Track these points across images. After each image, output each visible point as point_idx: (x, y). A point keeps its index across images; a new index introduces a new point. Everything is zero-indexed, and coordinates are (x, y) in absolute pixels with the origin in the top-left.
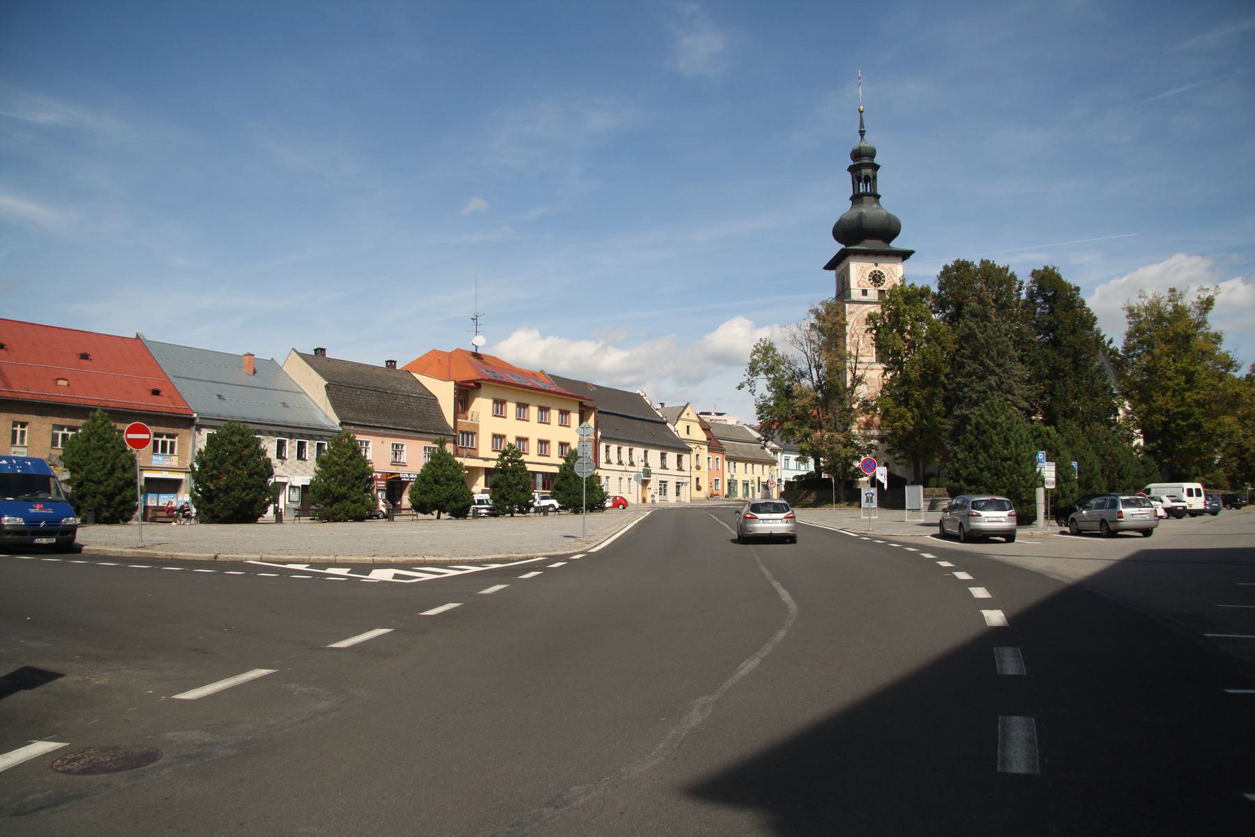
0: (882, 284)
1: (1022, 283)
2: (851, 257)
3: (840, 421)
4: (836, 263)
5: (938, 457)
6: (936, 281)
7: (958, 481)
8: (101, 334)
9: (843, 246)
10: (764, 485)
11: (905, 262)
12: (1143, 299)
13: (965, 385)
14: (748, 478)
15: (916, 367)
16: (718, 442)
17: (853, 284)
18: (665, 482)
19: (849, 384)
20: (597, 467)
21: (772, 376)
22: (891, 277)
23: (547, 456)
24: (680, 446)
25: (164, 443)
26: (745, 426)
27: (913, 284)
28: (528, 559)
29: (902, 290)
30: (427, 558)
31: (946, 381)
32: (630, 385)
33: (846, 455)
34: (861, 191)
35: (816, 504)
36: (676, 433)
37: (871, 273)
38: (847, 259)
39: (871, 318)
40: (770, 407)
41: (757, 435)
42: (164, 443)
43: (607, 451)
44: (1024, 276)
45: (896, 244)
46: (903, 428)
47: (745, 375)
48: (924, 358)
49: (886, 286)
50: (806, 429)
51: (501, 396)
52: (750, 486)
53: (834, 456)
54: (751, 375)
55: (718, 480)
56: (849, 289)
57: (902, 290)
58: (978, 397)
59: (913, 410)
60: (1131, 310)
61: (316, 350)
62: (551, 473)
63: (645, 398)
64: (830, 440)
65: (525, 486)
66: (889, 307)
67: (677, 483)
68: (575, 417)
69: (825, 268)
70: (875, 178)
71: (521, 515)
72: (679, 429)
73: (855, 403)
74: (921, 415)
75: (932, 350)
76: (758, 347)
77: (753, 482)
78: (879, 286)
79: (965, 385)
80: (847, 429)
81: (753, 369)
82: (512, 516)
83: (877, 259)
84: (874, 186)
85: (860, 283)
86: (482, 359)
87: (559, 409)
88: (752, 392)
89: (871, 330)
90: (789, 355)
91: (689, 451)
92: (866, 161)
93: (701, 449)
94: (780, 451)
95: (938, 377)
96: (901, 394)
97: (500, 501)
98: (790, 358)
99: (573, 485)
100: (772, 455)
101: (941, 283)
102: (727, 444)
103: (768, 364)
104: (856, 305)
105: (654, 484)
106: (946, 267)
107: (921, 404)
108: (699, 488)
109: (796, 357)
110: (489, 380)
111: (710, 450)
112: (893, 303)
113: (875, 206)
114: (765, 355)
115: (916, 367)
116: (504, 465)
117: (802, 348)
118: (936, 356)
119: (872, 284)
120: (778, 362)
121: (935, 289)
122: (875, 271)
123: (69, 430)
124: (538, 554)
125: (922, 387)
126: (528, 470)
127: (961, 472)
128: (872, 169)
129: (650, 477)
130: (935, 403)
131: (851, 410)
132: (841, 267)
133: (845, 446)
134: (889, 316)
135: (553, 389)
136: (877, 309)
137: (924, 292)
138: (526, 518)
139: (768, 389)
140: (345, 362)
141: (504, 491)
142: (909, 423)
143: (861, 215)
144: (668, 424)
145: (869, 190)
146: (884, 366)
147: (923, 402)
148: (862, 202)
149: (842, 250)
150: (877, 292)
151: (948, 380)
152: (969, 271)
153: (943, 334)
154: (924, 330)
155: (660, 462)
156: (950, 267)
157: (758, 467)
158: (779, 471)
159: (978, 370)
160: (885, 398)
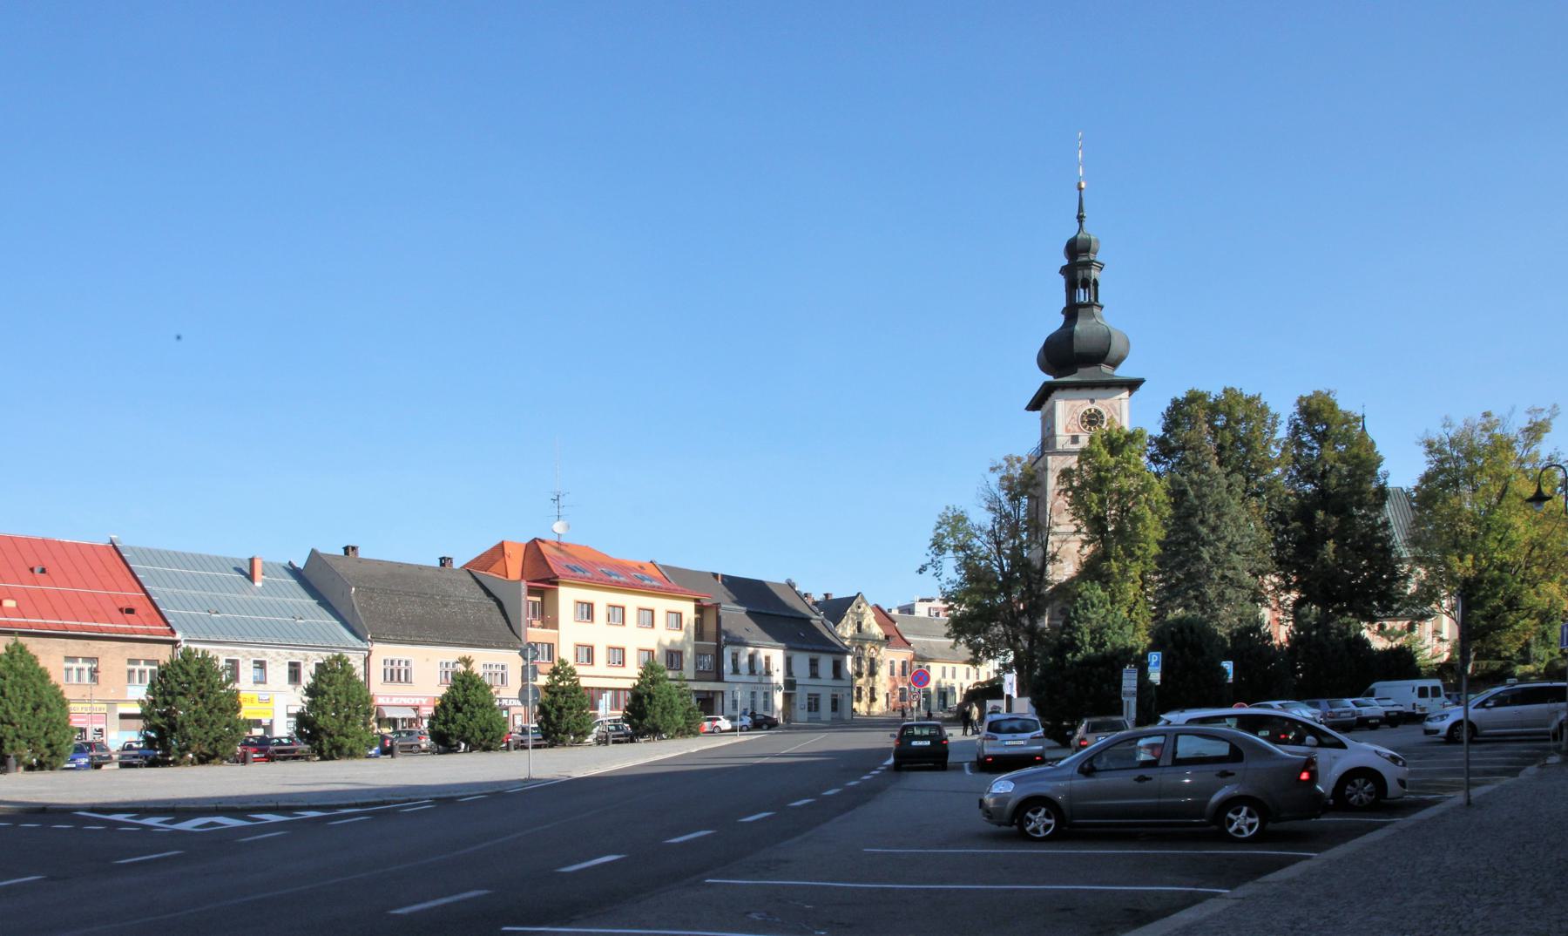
1: (1276, 416)
2: (1056, 394)
4: (1039, 401)
6: (1160, 421)
9: (1050, 378)
12: (1447, 430)
17: (1060, 430)
20: (719, 678)
44: (1283, 408)
47: (927, 555)
60: (1430, 445)
61: (346, 549)
81: (938, 545)
89: (1066, 491)
104: (1061, 458)
129: (794, 689)
139: (956, 571)
140: (380, 563)
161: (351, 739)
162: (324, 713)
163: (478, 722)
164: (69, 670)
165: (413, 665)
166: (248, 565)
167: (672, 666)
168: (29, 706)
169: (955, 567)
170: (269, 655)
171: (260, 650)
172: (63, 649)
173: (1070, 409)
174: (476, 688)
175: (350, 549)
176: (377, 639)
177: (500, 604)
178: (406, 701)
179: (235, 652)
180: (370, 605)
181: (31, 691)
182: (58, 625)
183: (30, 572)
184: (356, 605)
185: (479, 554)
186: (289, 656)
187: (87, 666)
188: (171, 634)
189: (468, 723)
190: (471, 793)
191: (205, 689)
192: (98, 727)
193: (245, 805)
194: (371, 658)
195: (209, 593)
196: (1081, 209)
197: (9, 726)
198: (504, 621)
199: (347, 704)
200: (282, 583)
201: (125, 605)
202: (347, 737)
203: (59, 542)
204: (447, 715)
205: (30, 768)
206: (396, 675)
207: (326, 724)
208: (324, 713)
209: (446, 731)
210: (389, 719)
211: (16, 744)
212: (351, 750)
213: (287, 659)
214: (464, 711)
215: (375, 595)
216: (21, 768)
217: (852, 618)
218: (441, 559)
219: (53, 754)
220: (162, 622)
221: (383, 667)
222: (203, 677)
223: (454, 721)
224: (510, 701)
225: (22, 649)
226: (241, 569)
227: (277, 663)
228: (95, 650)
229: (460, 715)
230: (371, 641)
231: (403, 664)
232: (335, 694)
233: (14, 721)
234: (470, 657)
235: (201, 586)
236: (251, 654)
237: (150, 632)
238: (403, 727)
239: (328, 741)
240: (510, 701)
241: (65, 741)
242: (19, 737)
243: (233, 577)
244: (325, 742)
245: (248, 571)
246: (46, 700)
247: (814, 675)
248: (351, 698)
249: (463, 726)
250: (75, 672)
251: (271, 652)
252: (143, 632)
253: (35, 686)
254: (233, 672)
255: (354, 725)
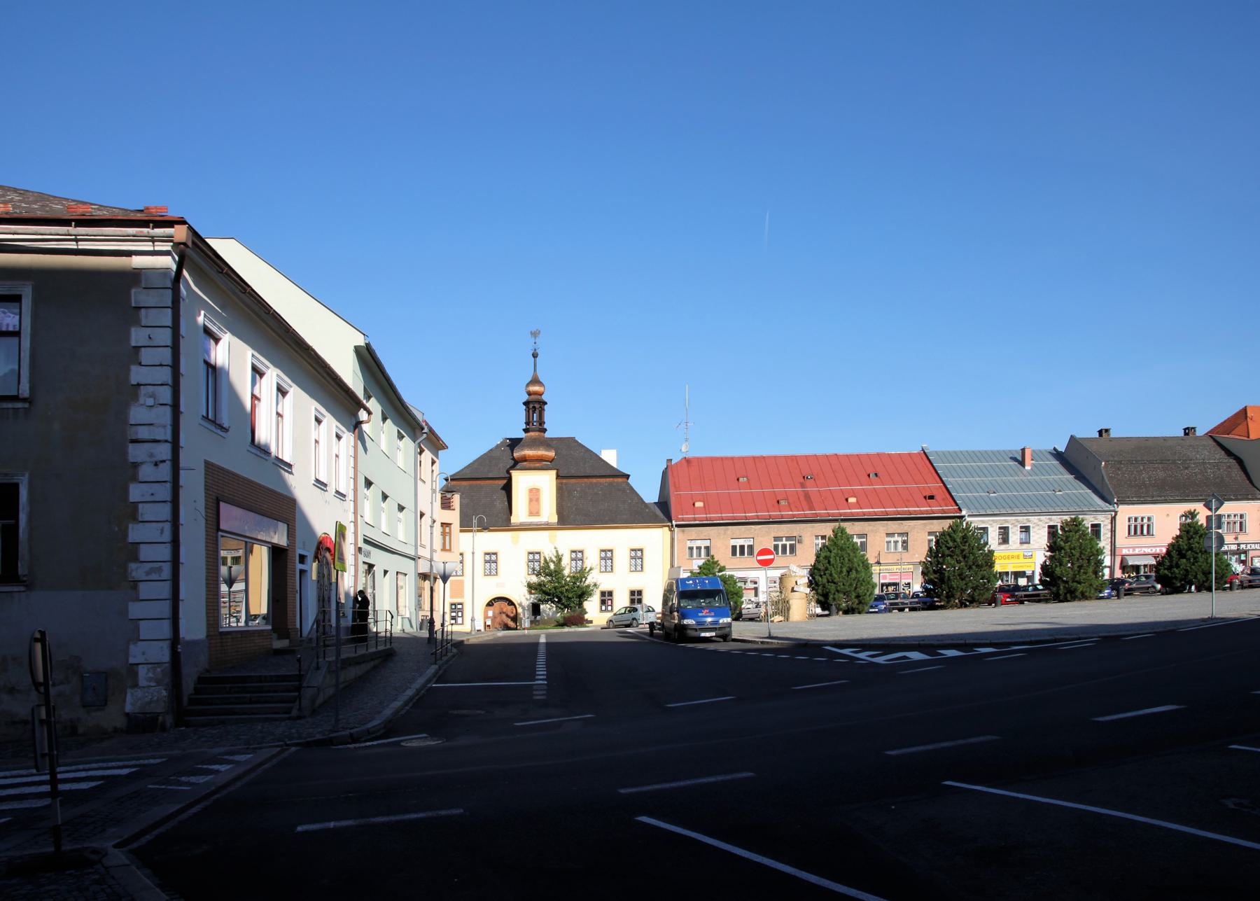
25: (784, 547)
42: (784, 547)
61: (1100, 432)
123: (786, 540)
161: (1083, 584)
162: (1061, 565)
163: (1200, 566)
164: (889, 542)
165: (1154, 520)
166: (1021, 454)
168: (844, 570)
170: (1033, 521)
171: (1025, 518)
172: (885, 528)
174: (1199, 537)
175: (1104, 431)
176: (1122, 502)
177: (1240, 462)
178: (1148, 551)
179: (1006, 521)
180: (1118, 475)
181: (846, 559)
182: (882, 511)
183: (868, 477)
184: (1105, 478)
185: (1222, 420)
186: (1048, 521)
187: (900, 539)
188: (958, 511)
189: (1191, 568)
190: (1140, 632)
191: (967, 551)
192: (907, 581)
193: (941, 642)
194: (1117, 517)
195: (990, 479)
197: (832, 584)
198: (1244, 476)
199: (1080, 557)
200: (1047, 465)
201: (928, 494)
202: (1079, 583)
203: (888, 454)
204: (1171, 561)
205: (846, 612)
206: (1140, 529)
207: (1062, 574)
208: (1061, 565)
209: (1170, 575)
210: (1132, 566)
211: (836, 596)
212: (1083, 593)
213: (1046, 523)
214: (1188, 557)
215: (1122, 466)
216: (841, 613)
218: (1185, 429)
219: (860, 603)
220: (954, 504)
221: (1127, 524)
222: (966, 542)
223: (1178, 566)
224: (1249, 546)
225: (843, 531)
226: (1015, 458)
227: (1038, 527)
228: (906, 527)
229: (1184, 560)
230: (1117, 504)
231: (1145, 520)
232: (1071, 549)
233: (835, 581)
234: (1195, 510)
235: (1010, 474)
236: (1017, 521)
237: (944, 512)
238: (1145, 572)
239: (1064, 587)
240: (1249, 546)
241: (868, 594)
242: (838, 591)
243: (1009, 465)
244: (1062, 587)
245: (1020, 459)
246: (856, 565)
248: (1083, 552)
249: (1186, 570)
250: (892, 544)
251: (1034, 519)
252: (939, 512)
253: (849, 556)
254: (1004, 536)
255: (1085, 573)
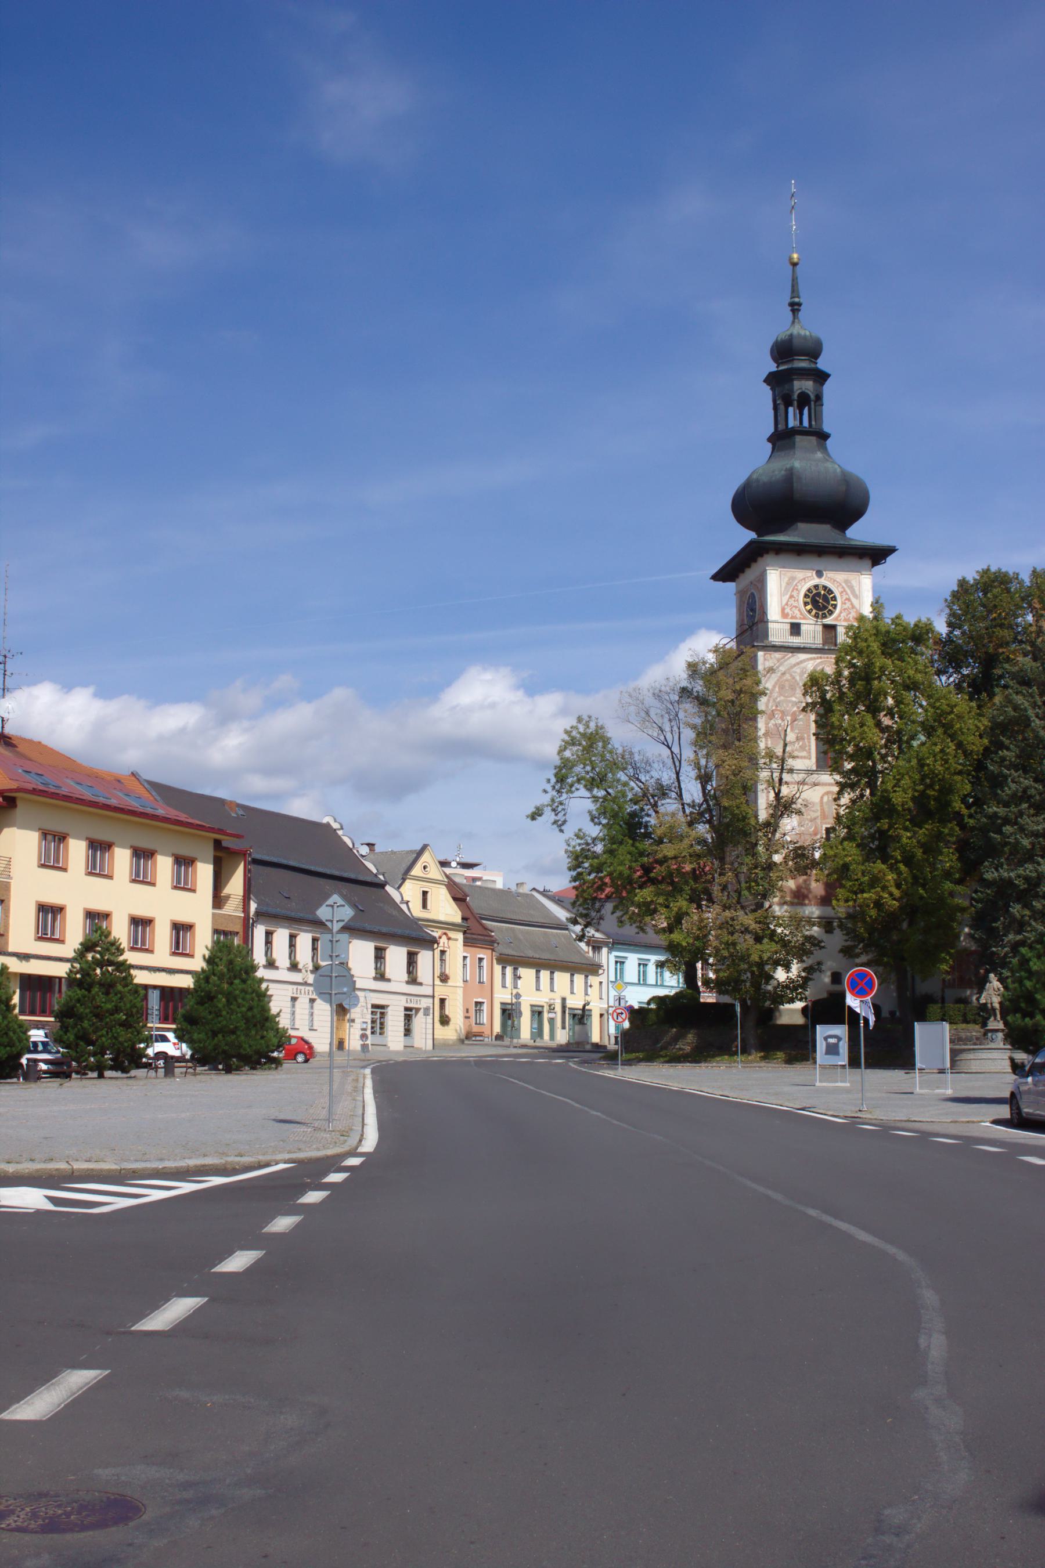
0: (831, 613)
2: (768, 558)
3: (749, 888)
5: (946, 961)
6: (942, 611)
7: (1032, 1016)
8: (367, 867)
9: (751, 535)
10: (574, 1015)
11: (876, 568)
13: (1006, 821)
14: (542, 998)
15: (906, 782)
16: (481, 924)
18: (382, 1007)
19: (763, 815)
21: (601, 793)
22: (849, 599)
23: (147, 951)
24: (414, 934)
26: (535, 894)
27: (898, 617)
28: (261, 1166)
29: (876, 628)
30: (76, 1166)
31: (964, 811)
32: (277, 796)
33: (761, 958)
34: (791, 424)
35: (699, 1055)
36: (404, 907)
37: (809, 590)
38: (761, 561)
39: (814, 682)
40: (595, 856)
41: (562, 914)
43: (268, 942)
45: (859, 533)
46: (878, 904)
47: (545, 791)
48: (921, 764)
49: (841, 618)
50: (681, 903)
51: (56, 825)
52: (546, 1016)
53: (732, 959)
54: (558, 792)
55: (481, 1003)
56: (764, 620)
57: (876, 628)
58: (1033, 844)
59: (897, 869)
62: (181, 989)
63: (340, 833)
64: (727, 926)
65: (130, 1015)
66: (850, 662)
67: (407, 1009)
68: (204, 872)
69: (716, 577)
70: (819, 398)
71: (119, 1074)
72: (408, 895)
73: (776, 852)
74: (915, 878)
75: (937, 749)
76: (574, 733)
77: (551, 1008)
78: (824, 616)
79: (1006, 821)
80: (761, 905)
81: (562, 778)
82: (101, 1076)
83: (820, 563)
84: (816, 416)
85: (787, 610)
86: (14, 746)
87: (131, 847)
88: (560, 825)
89: (813, 705)
90: (635, 750)
91: (430, 943)
92: (802, 364)
93: (449, 939)
94: (606, 944)
95: (948, 804)
96: (872, 837)
97: (77, 1045)
98: (637, 757)
99: (224, 1013)
100: (591, 954)
101: (953, 614)
102: (500, 929)
103: (593, 768)
104: (778, 655)
105: (361, 1014)
106: (962, 583)
107: (913, 856)
108: (445, 1021)
109: (649, 755)
110: (35, 791)
111: (468, 942)
112: (860, 653)
113: (819, 455)
114: (589, 749)
115: (906, 782)
116: (86, 972)
117: (662, 738)
118: (946, 761)
119: (810, 612)
120: (615, 766)
121: (941, 627)
122: (816, 587)
124: (279, 1157)
125: (916, 823)
126: (136, 981)
127: (1038, 996)
128: (815, 381)
130: (941, 853)
131: (770, 866)
132: (749, 576)
133: (758, 939)
134: (852, 680)
135: (161, 812)
136: (827, 665)
137: (920, 634)
138: (125, 1081)
139: (592, 820)
141: (86, 1024)
142: (891, 894)
143: (790, 476)
144: (388, 888)
145: (806, 423)
146: (838, 777)
147: (919, 853)
148: (792, 446)
149: (751, 543)
150: (820, 628)
151: (968, 807)
152: (1008, 591)
153: (960, 717)
154: (920, 708)
155: (373, 965)
156: (972, 582)
157: (562, 978)
158: (604, 985)
159: (1032, 792)
160: (841, 843)
167: (178, 949)
169: (590, 812)
173: (788, 584)
196: (795, 291)
217: (854, 885)
247: (381, 976)
